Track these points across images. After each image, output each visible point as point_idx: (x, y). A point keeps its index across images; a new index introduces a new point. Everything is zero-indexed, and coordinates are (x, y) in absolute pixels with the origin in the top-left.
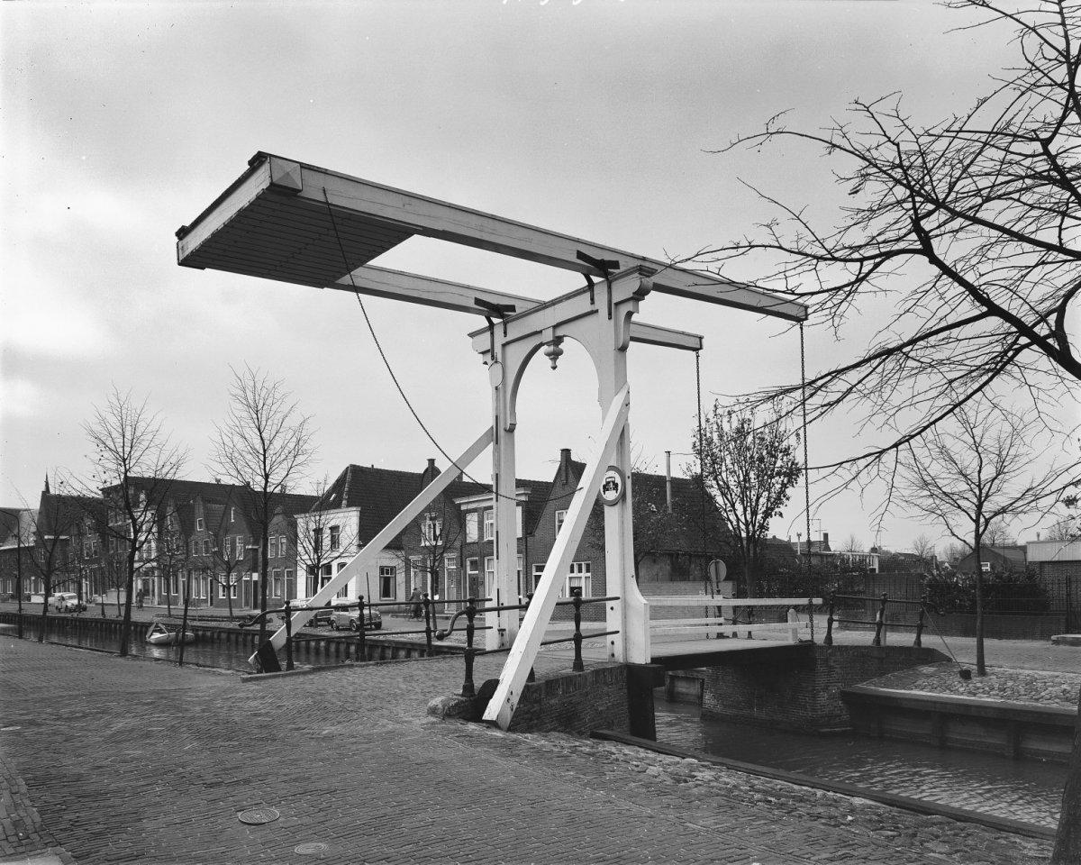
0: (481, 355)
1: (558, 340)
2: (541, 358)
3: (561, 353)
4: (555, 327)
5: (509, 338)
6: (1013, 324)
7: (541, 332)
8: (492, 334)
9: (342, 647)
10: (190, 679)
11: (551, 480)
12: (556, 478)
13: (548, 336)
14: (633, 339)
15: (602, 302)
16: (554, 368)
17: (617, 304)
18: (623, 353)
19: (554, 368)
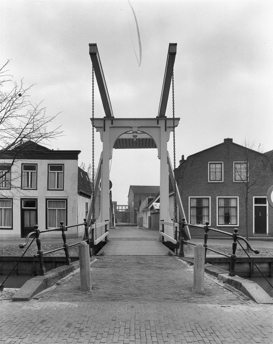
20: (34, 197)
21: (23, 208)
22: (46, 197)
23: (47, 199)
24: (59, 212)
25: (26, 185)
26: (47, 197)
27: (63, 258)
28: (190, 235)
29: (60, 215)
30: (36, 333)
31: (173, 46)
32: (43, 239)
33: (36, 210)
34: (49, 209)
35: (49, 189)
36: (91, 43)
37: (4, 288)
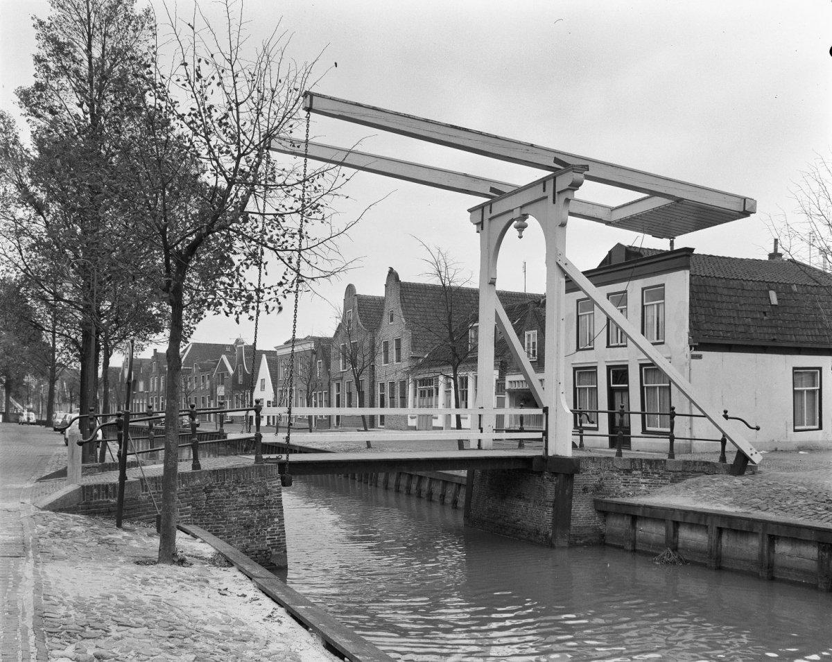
0: (475, 226)
1: (525, 217)
2: (512, 231)
3: (526, 226)
4: (521, 207)
5: (494, 214)
6: (181, 315)
7: (512, 210)
8: (483, 211)
9: (450, 491)
10: (37, 294)
11: (330, 333)
12: (337, 332)
13: (517, 214)
14: (571, 214)
15: (549, 192)
16: (520, 237)
17: (559, 193)
18: (563, 228)
19: (520, 237)
20: (589, 363)
21: (612, 385)
22: (639, 360)
23: (575, 369)
24: (662, 392)
25: (615, 340)
26: (575, 364)
27: (282, 444)
28: (228, 404)
29: (325, 396)
30: (41, 458)
31: (554, 203)
32: (637, 452)
33: (627, 390)
34: (647, 387)
35: (611, 345)
36: (470, 207)
37: (161, 473)
